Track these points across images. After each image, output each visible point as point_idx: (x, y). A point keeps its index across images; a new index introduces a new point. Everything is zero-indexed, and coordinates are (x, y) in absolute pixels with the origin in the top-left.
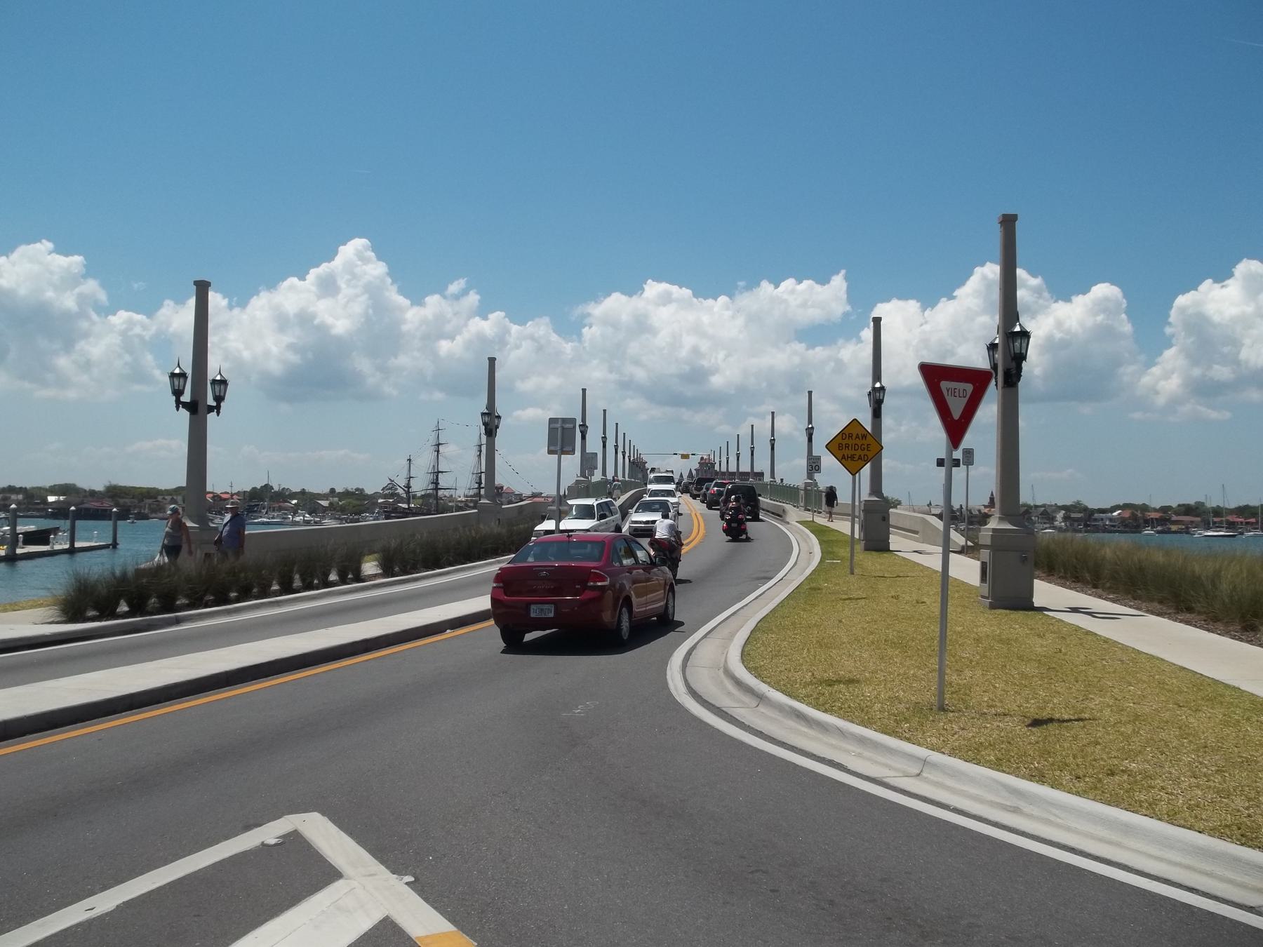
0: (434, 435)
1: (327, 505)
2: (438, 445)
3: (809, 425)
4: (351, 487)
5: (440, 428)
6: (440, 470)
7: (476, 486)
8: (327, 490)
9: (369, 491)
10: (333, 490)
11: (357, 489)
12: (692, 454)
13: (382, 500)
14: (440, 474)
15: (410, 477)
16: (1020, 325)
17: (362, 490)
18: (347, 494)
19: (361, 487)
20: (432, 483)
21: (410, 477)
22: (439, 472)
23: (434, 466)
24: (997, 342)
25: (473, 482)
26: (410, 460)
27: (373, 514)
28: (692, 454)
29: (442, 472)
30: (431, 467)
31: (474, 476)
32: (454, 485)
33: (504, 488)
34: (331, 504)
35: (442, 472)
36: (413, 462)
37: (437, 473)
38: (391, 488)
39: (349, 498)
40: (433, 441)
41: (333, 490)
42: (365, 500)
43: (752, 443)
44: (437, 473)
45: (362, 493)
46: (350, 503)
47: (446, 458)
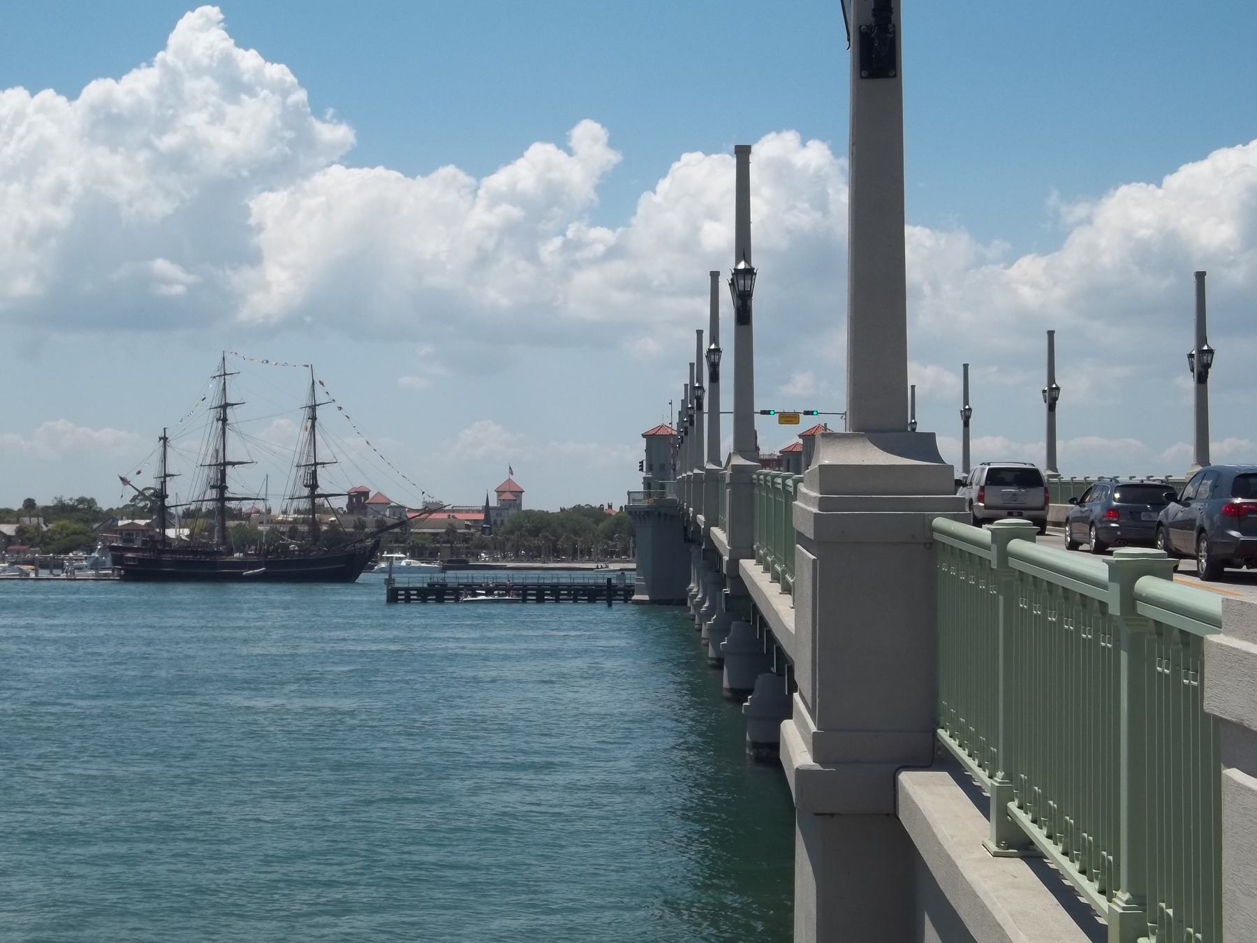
0: (213, 387)
1: (14, 534)
2: (225, 406)
3: (738, 262)
4: (70, 494)
5: (227, 372)
6: (229, 458)
7: (306, 492)
8: (17, 505)
9: (104, 504)
10: (30, 504)
11: (82, 500)
12: (807, 413)
13: (127, 522)
14: (168, 479)
15: (166, 476)
16: (1207, 345)
17: (91, 502)
18: (62, 510)
19: (88, 496)
20: (213, 487)
21: (166, 476)
22: (226, 464)
23: (217, 451)
24: (1194, 353)
25: (300, 483)
26: (164, 439)
27: (92, 551)
28: (807, 413)
29: (233, 464)
30: (211, 451)
31: (302, 470)
32: (263, 492)
33: (371, 495)
34: (20, 531)
35: (233, 464)
36: (172, 443)
37: (222, 466)
38: (227, 488)
39: (66, 518)
40: (305, 400)
41: (30, 504)
42: (95, 521)
43: (966, 402)
44: (222, 466)
45: (91, 507)
46: (63, 528)
47: (241, 434)
